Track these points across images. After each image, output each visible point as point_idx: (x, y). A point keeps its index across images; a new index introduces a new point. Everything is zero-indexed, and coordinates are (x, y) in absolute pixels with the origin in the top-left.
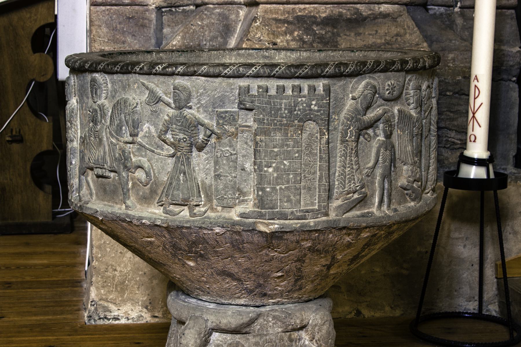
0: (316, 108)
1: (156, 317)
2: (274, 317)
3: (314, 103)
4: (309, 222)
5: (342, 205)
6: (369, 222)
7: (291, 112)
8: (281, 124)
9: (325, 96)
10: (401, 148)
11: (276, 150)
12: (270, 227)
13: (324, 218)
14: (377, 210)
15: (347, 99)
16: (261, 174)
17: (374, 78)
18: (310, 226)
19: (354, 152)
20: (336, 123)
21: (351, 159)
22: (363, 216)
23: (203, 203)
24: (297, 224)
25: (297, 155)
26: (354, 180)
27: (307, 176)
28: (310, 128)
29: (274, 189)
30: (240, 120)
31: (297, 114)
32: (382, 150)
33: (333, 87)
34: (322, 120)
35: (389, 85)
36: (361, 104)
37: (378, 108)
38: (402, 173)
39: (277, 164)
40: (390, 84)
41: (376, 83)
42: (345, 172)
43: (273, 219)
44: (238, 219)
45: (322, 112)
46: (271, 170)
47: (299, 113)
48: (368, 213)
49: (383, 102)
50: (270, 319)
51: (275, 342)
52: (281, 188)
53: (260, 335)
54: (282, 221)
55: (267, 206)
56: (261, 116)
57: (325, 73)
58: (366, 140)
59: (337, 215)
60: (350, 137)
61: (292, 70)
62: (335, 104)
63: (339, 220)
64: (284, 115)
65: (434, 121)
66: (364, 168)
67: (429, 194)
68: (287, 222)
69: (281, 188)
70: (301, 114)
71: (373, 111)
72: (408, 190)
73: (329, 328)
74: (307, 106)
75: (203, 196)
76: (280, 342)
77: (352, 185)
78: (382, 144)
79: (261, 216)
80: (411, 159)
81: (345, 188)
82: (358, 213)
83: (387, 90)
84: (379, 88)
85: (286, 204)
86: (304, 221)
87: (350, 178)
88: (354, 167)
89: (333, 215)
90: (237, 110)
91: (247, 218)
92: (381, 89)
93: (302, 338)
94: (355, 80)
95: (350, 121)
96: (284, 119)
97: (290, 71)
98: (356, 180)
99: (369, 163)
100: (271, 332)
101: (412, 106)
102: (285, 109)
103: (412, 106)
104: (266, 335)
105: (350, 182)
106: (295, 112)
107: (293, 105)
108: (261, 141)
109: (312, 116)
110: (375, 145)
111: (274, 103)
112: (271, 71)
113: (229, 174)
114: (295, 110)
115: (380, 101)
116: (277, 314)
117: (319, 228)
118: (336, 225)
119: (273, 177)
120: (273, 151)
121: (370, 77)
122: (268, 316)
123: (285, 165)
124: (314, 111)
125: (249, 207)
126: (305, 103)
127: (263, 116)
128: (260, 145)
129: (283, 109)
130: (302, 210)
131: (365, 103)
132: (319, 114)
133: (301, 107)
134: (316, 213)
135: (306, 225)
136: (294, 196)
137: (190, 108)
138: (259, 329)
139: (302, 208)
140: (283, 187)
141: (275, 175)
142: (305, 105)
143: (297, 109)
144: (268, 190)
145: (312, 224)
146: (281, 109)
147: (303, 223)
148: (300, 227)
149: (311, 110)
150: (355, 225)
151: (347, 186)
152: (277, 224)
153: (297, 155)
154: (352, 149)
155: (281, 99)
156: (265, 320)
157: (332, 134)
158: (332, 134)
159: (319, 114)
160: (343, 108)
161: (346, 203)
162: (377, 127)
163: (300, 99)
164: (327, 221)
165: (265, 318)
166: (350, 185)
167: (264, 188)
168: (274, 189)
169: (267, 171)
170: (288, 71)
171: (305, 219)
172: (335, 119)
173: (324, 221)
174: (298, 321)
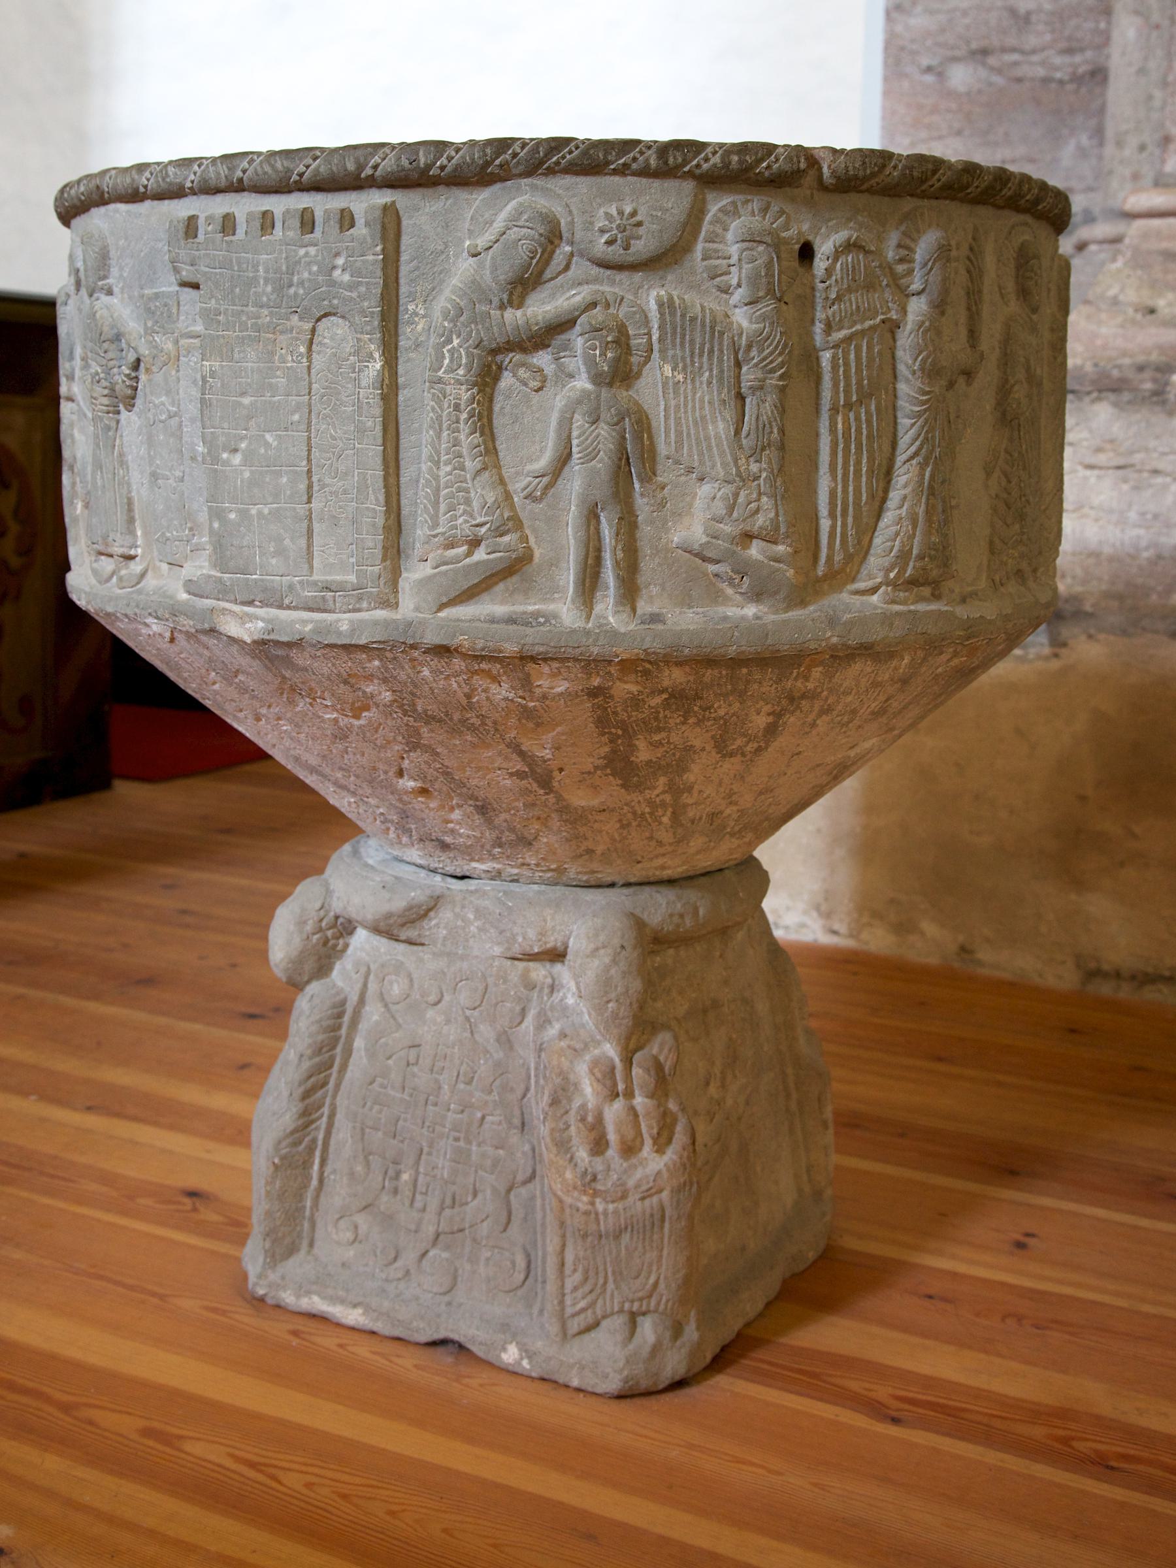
0: (346, 277)
1: (835, 933)
2: (479, 913)
3: (340, 261)
4: (339, 620)
5: (430, 578)
6: (529, 640)
7: (281, 287)
8: (256, 323)
9: (369, 240)
10: (678, 423)
11: (246, 401)
12: (247, 626)
13: (381, 614)
14: (616, 613)
15: (457, 256)
16: (216, 470)
17: (545, 191)
18: (339, 634)
19: (464, 416)
20: (420, 327)
21: (456, 439)
22: (511, 620)
23: (139, 551)
24: (305, 622)
25: (296, 417)
26: (468, 501)
27: (328, 481)
28: (332, 339)
29: (243, 513)
30: (182, 318)
31: (296, 294)
32: (579, 420)
33: (411, 217)
34: (363, 313)
35: (608, 216)
36: (494, 268)
37: (572, 287)
38: (691, 506)
39: (250, 443)
40: (614, 212)
41: (558, 210)
42: (437, 478)
43: (250, 603)
44: (184, 596)
45: (363, 289)
46: (237, 459)
47: (301, 291)
48: (536, 615)
49: (595, 270)
50: (471, 916)
51: (484, 977)
52: (260, 513)
53: (448, 954)
54: (273, 612)
55: (232, 564)
56: (213, 301)
57: (368, 171)
58: (526, 385)
59: (417, 609)
60: (450, 370)
61: (279, 165)
62: (417, 268)
63: (422, 623)
64: (265, 299)
65: (908, 367)
66: (517, 473)
67: (875, 598)
68: (284, 615)
69: (260, 513)
70: (307, 294)
71: (553, 296)
72: (718, 562)
73: (607, 969)
74: (319, 271)
75: (139, 533)
76: (496, 985)
77: (461, 520)
78: (579, 402)
79: (224, 592)
80: (725, 465)
81: (436, 525)
82: (501, 610)
83: (602, 231)
84: (572, 223)
85: (274, 561)
86: (325, 615)
87: (451, 496)
88: (468, 464)
89: (408, 606)
90: (177, 288)
91: (202, 597)
92: (578, 226)
93: (563, 986)
94: (485, 194)
95: (451, 321)
96: (265, 312)
97: (273, 166)
98: (475, 503)
99: (538, 458)
100: (476, 952)
101: (738, 295)
102: (266, 280)
103: (738, 295)
104: (463, 958)
105: (452, 508)
106: (292, 291)
107: (284, 268)
108: (213, 374)
109: (335, 302)
110: (558, 399)
111: (239, 264)
112: (229, 169)
113: (170, 470)
114: (290, 286)
115: (580, 268)
116: (486, 903)
117: (363, 641)
118: (413, 637)
119: (242, 481)
120: (240, 404)
121: (534, 187)
122: (463, 907)
123: (267, 445)
124: (340, 285)
125: (200, 567)
126: (316, 263)
127: (217, 300)
128: (211, 387)
129: (262, 282)
130: (315, 583)
131: (507, 268)
132: (354, 295)
133: (306, 275)
134: (356, 597)
135: (329, 629)
136: (292, 539)
137: (110, 292)
138: (445, 939)
139: (315, 577)
140: (266, 511)
141: (247, 475)
142: (315, 268)
143: (295, 279)
144: (232, 516)
145: (344, 627)
146: (255, 278)
147: (320, 622)
148: (314, 631)
149: (333, 283)
150: (479, 646)
151: (442, 519)
152: (263, 620)
153: (296, 417)
154: (457, 407)
155: (256, 252)
156: (457, 916)
157: (409, 360)
158: (409, 360)
159: (354, 295)
160: (442, 281)
161: (445, 573)
162: (566, 347)
163: (302, 252)
164: (387, 623)
165: (457, 910)
166: (455, 518)
167: (223, 510)
168: (243, 513)
169: (227, 463)
170: (267, 168)
171: (325, 611)
172: (416, 314)
173: (376, 623)
174: (532, 934)
